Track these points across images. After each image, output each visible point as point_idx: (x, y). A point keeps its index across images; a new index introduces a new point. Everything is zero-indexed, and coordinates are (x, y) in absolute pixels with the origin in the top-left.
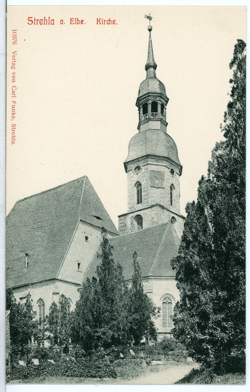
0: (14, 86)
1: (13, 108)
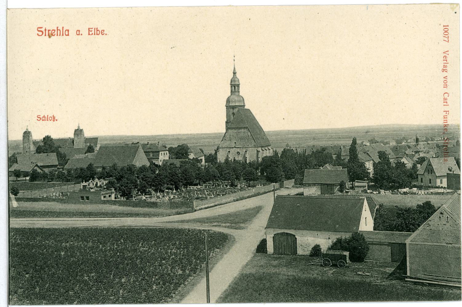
0: (445, 92)
1: (445, 119)
